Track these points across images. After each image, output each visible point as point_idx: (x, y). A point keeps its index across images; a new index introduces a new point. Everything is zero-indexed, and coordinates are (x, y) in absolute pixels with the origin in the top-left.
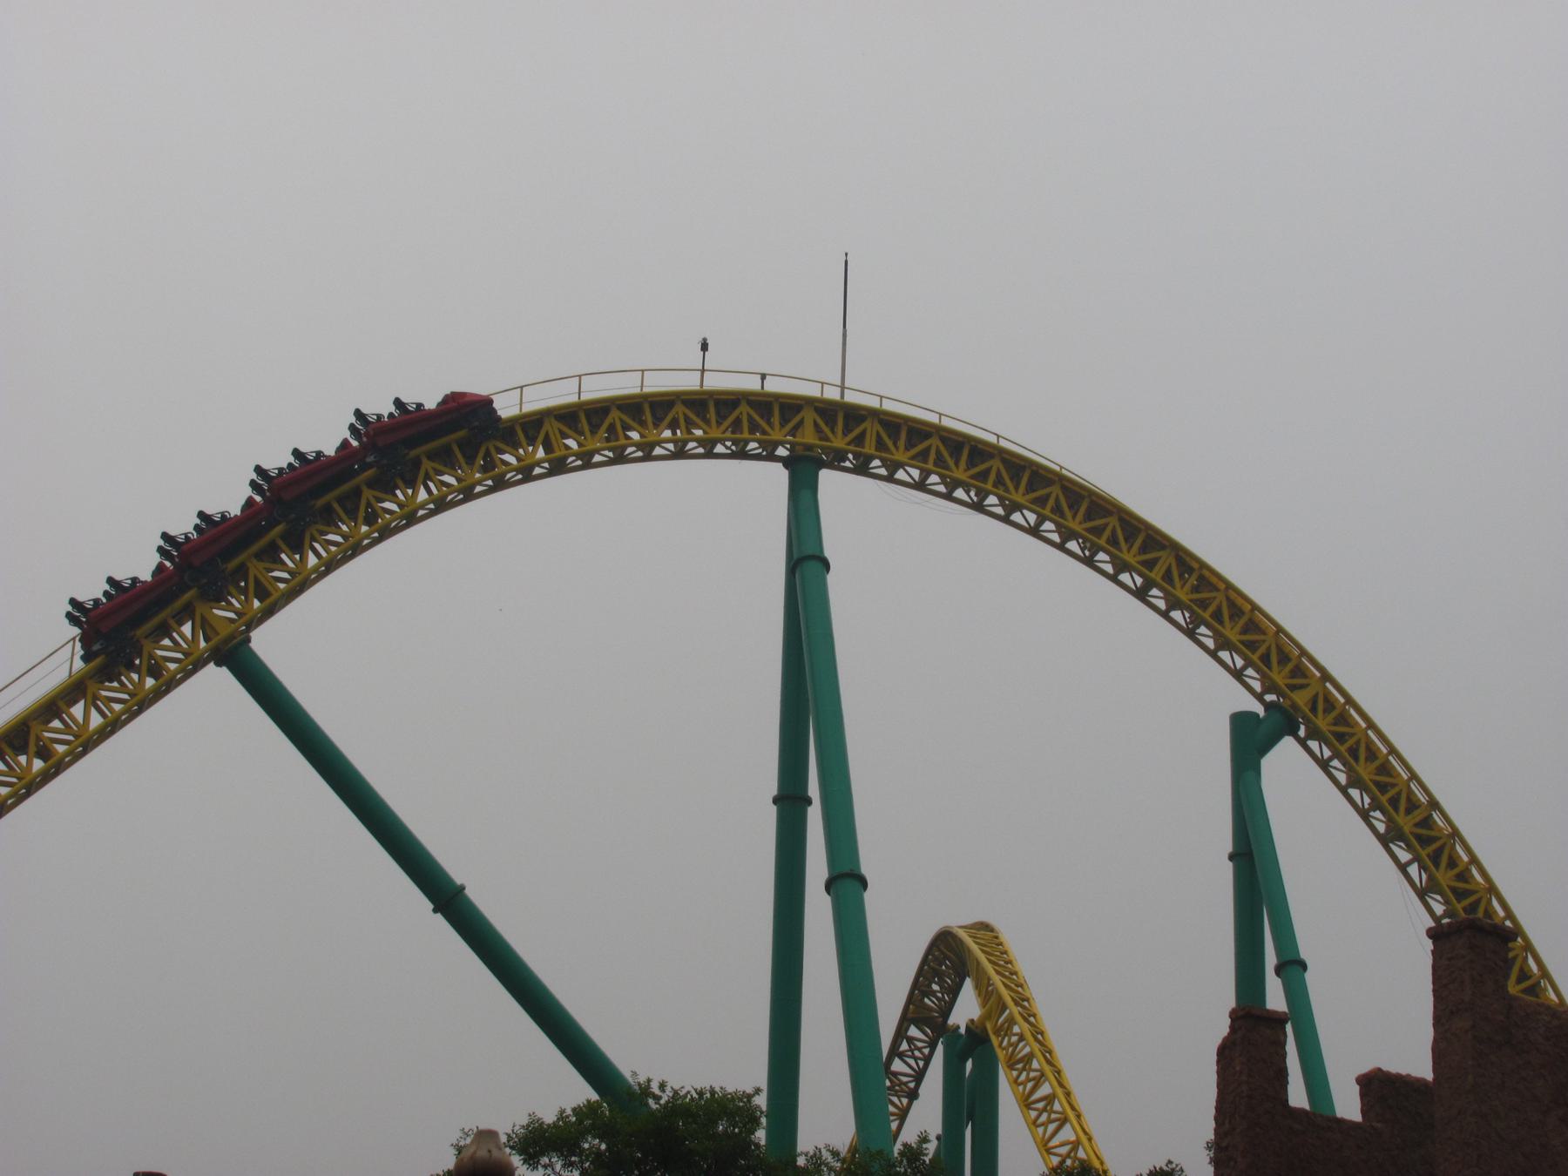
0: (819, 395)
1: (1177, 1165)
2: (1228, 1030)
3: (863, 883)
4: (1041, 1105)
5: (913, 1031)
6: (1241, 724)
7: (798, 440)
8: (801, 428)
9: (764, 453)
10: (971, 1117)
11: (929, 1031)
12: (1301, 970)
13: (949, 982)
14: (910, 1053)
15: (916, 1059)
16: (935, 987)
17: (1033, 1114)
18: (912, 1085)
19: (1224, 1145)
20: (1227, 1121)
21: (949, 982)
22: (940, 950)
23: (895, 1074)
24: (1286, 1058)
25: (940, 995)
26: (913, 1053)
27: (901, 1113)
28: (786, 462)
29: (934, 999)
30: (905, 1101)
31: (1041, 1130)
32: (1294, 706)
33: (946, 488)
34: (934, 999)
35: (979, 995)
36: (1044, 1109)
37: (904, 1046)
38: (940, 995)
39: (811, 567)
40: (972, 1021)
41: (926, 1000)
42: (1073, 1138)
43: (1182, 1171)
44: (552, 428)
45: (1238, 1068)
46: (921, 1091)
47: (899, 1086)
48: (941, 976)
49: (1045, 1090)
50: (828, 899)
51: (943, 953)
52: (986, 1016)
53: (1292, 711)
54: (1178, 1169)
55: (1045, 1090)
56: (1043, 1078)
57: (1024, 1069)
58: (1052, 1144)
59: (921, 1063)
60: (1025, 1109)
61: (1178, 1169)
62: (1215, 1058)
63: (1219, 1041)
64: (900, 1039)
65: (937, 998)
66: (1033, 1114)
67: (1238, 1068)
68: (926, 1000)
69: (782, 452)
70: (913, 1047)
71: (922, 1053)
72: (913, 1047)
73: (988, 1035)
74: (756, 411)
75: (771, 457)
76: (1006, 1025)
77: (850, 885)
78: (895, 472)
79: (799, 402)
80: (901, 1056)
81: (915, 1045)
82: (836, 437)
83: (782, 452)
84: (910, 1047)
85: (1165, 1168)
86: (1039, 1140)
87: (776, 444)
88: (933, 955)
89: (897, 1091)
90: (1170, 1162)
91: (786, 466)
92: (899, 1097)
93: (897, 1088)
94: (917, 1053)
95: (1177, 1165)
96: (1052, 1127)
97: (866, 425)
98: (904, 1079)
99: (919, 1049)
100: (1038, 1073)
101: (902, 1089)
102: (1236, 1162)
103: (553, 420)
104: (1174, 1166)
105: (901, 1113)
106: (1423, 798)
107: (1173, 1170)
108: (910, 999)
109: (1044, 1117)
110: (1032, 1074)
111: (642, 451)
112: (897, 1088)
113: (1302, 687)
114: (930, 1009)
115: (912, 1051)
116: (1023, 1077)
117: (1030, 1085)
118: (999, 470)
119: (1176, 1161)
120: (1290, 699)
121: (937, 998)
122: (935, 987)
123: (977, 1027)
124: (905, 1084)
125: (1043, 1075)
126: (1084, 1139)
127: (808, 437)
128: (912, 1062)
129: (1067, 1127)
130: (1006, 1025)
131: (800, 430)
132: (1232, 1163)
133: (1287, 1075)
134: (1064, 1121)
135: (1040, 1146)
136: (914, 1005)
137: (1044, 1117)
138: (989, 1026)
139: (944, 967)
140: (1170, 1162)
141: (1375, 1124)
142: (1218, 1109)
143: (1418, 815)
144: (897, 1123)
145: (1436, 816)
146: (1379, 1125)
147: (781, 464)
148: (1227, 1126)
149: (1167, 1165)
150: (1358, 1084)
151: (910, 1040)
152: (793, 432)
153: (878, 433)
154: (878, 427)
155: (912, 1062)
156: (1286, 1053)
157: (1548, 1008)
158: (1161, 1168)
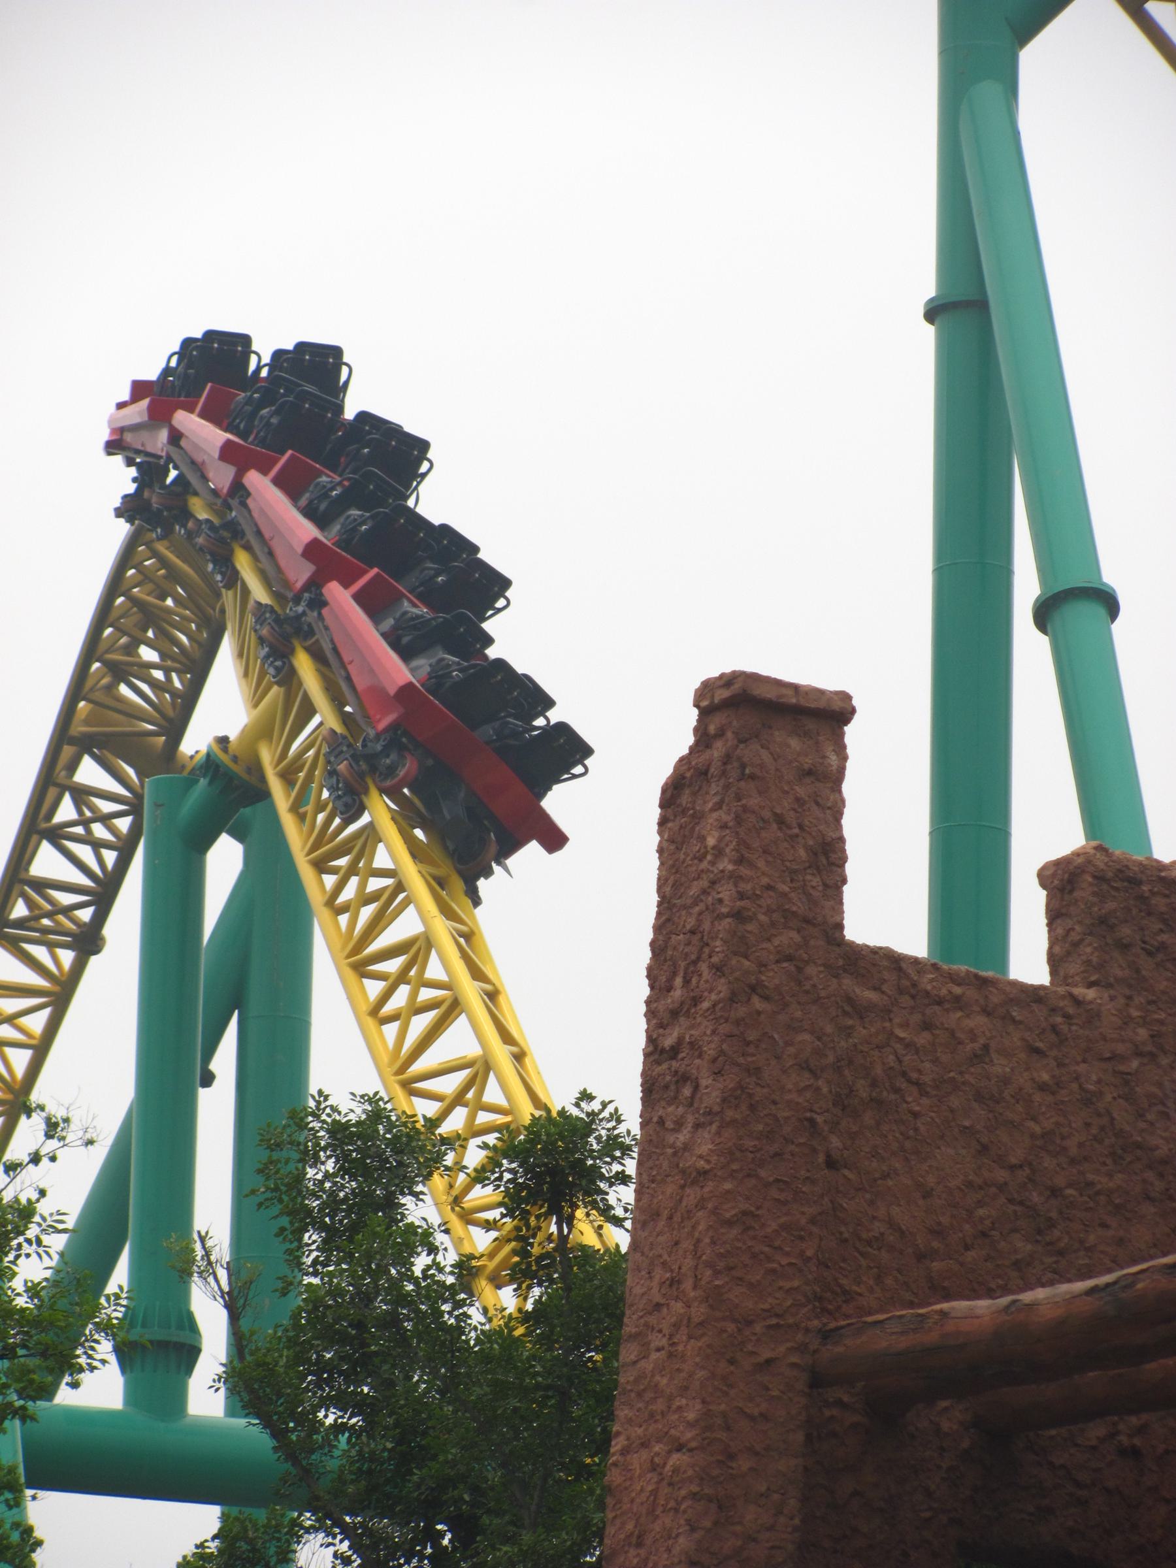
1: (604, 1105)
2: (690, 740)
3: (1110, 604)
4: (392, 966)
5: (89, 773)
11: (131, 772)
12: (1101, 612)
13: (184, 639)
14: (79, 830)
15: (97, 845)
16: (148, 654)
17: (374, 988)
18: (85, 915)
19: (668, 1042)
20: (678, 981)
21: (184, 639)
22: (155, 554)
23: (42, 885)
24: (841, 814)
25: (158, 675)
26: (89, 831)
27: (57, 989)
29: (145, 687)
30: (67, 957)
31: (391, 1031)
34: (145, 687)
35: (246, 674)
36: (402, 977)
37: (66, 811)
38: (158, 675)
40: (223, 741)
41: (124, 689)
42: (473, 1050)
43: (619, 1121)
45: (711, 841)
46: (108, 930)
47: (49, 915)
48: (150, 616)
49: (405, 927)
50: (1044, 641)
51: (163, 562)
52: (261, 731)
54: (606, 1114)
55: (405, 927)
56: (401, 896)
57: (352, 870)
58: (419, 1066)
59: (110, 857)
60: (351, 975)
61: (606, 1114)
62: (654, 813)
63: (665, 771)
64: (52, 792)
65: (153, 684)
66: (374, 988)
67: (711, 841)
68: (124, 689)
70: (88, 814)
71: (113, 830)
72: (88, 814)
73: (263, 779)
76: (311, 753)
77: (1088, 612)
80: (56, 836)
81: (93, 808)
84: (80, 812)
85: (575, 1112)
86: (385, 1059)
88: (139, 566)
89: (45, 931)
90: (586, 1096)
92: (51, 946)
93: (46, 922)
94: (99, 831)
95: (604, 1105)
96: (420, 1024)
98: (66, 899)
100: (388, 882)
101: (57, 923)
102: (696, 1088)
104: (595, 1106)
105: (57, 989)
107: (592, 1115)
108: (78, 688)
109: (400, 998)
110: (375, 884)
112: (46, 922)
114: (133, 713)
115: (86, 823)
116: (349, 893)
117: (367, 912)
119: (601, 1095)
121: (153, 684)
122: (148, 654)
123: (235, 759)
124: (67, 910)
125: (400, 887)
126: (501, 1054)
128: (84, 852)
129: (460, 1027)
130: (311, 753)
132: (687, 1091)
133: (844, 859)
134: (451, 1009)
135: (389, 1071)
136: (89, 701)
137: (400, 998)
138: (267, 757)
139: (169, 602)
140: (586, 1096)
141: (1079, 991)
142: (658, 948)
144: (43, 1016)
146: (1091, 994)
148: (677, 993)
149: (577, 1105)
150: (1043, 885)
151: (82, 795)
156: (843, 801)
158: (562, 1113)
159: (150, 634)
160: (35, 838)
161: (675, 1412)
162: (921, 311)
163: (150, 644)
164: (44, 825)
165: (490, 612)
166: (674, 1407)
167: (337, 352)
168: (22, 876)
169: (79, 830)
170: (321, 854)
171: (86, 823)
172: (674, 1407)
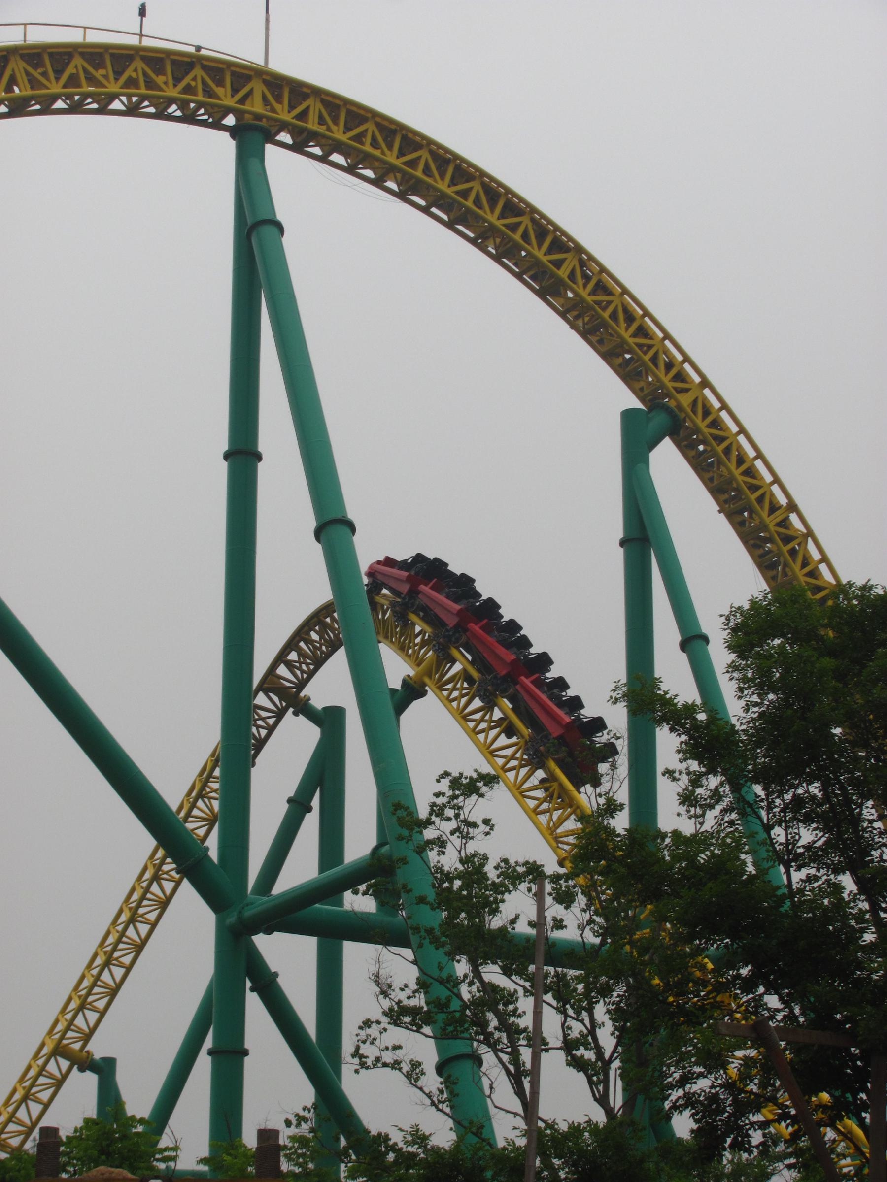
0: (262, 63)
6: (628, 416)
7: (247, 107)
8: (250, 97)
9: (211, 120)
10: (320, 785)
15: (302, 672)
21: (331, 635)
28: (233, 132)
29: (310, 646)
32: (680, 407)
33: (375, 174)
34: (310, 646)
39: (269, 231)
44: (18, 66)
53: (677, 411)
59: (305, 676)
65: (315, 647)
69: (230, 120)
71: (308, 668)
74: (269, 90)
75: (217, 125)
78: (330, 154)
79: (221, 66)
80: (308, 642)
82: (110, 83)
83: (230, 120)
87: (227, 111)
91: (233, 136)
94: (304, 667)
97: (309, 102)
99: (307, 665)
103: (18, 58)
106: (783, 501)
111: (98, 103)
113: (687, 390)
115: (301, 663)
118: (427, 160)
120: (676, 400)
127: (256, 106)
128: (298, 673)
131: (249, 99)
143: (778, 516)
145: (793, 518)
147: (228, 134)
152: (242, 101)
153: (320, 112)
154: (319, 106)
155: (298, 673)
157: (834, 631)
159: (317, 628)
160: (280, 662)
161: (453, 808)
162: (618, 543)
163: (316, 632)
164: (321, 618)
165: (317, 151)
166: (452, 803)
167: (551, 663)
168: (273, 673)
169: (297, 665)
170: (332, 910)
171: (301, 663)
172: (452, 803)
